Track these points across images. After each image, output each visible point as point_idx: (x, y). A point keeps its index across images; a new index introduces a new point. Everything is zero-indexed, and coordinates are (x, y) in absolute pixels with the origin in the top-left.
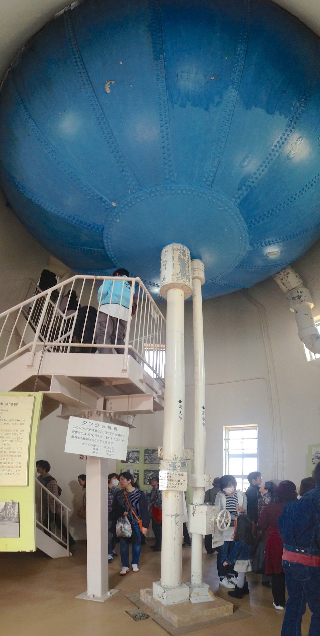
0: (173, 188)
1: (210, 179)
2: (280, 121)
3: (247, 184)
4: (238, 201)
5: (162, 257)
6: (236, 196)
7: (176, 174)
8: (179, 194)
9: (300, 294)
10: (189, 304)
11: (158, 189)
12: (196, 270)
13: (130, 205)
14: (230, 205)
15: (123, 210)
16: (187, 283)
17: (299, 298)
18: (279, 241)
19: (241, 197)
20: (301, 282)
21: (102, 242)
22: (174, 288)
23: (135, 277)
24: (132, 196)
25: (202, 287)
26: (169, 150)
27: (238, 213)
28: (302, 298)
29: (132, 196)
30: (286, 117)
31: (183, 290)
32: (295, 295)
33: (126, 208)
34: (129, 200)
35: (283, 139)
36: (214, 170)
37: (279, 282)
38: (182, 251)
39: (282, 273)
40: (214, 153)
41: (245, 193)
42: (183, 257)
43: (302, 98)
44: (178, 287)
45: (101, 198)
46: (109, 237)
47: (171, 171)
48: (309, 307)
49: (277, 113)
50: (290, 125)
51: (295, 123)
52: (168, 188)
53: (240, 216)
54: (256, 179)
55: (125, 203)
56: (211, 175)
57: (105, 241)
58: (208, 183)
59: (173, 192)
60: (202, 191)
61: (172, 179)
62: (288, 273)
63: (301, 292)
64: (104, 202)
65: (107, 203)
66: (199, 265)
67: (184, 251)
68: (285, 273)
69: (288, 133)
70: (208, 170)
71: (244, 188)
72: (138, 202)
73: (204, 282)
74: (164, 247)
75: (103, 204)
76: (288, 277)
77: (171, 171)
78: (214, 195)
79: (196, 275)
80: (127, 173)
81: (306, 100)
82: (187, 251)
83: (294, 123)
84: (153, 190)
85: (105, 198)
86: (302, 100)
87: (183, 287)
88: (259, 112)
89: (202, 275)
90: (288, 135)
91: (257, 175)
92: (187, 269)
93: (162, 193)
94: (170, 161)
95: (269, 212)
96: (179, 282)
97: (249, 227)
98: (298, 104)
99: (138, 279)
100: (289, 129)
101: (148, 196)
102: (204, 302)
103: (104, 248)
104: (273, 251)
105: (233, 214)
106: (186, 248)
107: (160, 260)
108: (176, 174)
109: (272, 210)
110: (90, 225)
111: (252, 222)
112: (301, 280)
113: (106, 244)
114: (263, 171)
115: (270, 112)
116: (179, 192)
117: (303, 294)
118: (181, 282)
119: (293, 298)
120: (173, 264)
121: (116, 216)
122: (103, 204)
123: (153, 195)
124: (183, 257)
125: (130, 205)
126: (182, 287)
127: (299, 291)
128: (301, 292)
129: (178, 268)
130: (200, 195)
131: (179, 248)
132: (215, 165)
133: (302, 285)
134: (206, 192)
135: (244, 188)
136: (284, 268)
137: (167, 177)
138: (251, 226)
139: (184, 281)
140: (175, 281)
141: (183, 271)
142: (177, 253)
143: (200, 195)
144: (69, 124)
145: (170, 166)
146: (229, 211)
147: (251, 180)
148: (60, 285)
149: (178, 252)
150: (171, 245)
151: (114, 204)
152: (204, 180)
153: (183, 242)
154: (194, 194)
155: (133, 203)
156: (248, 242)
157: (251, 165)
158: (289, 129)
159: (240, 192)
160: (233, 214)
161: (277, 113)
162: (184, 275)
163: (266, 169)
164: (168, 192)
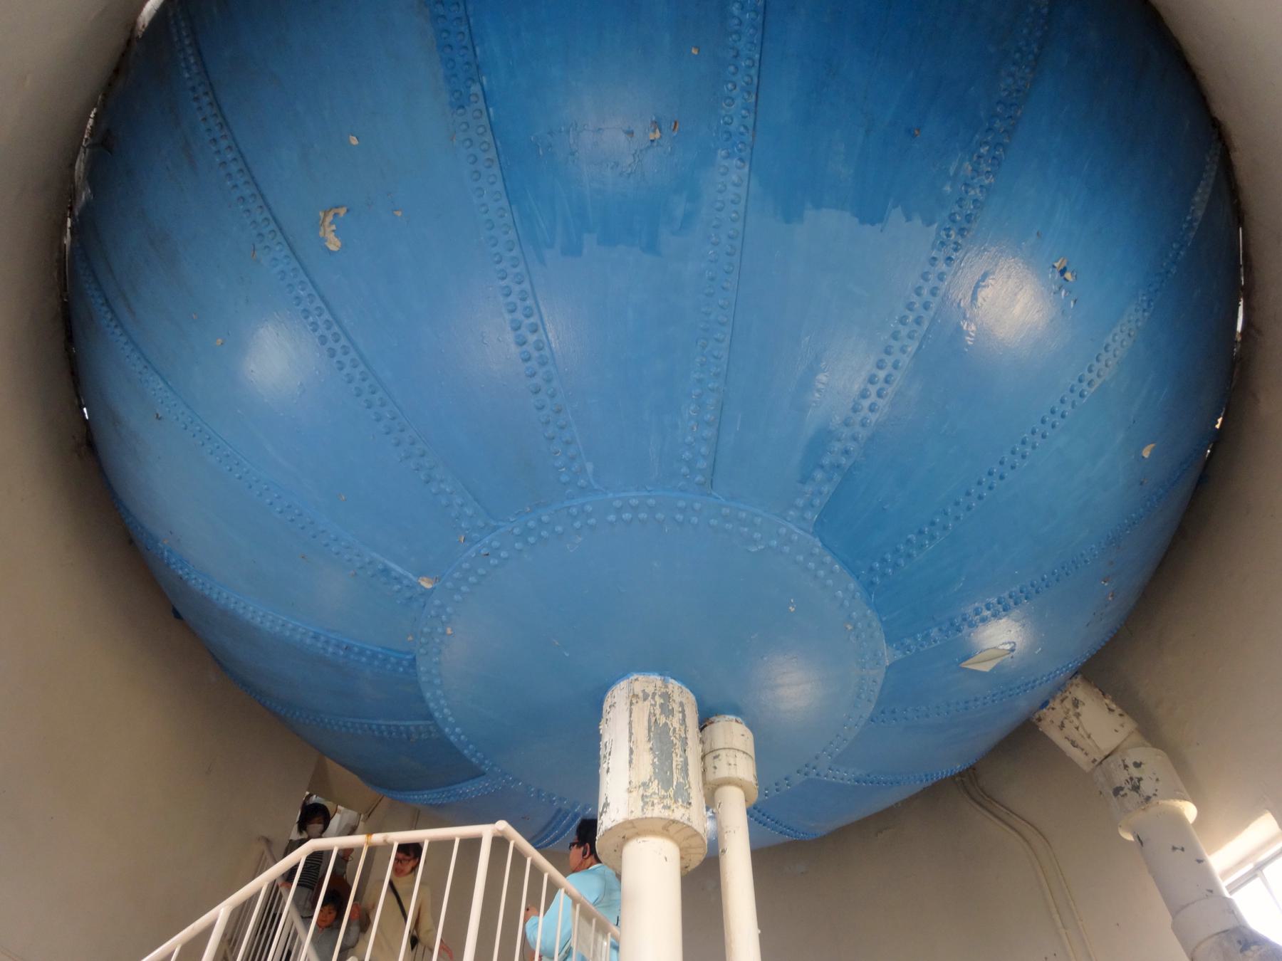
0: (589, 508)
1: (702, 464)
2: (908, 237)
3: (826, 461)
4: (812, 516)
5: (603, 727)
6: (800, 502)
7: (590, 467)
8: (611, 523)
9: (1135, 772)
10: (701, 883)
11: (545, 518)
12: (723, 753)
13: (472, 579)
14: (783, 531)
15: (457, 597)
16: (679, 813)
17: (1136, 788)
18: (987, 613)
19: (817, 502)
20: (1130, 725)
21: (422, 699)
22: (638, 834)
23: (492, 820)
24: (472, 553)
25: (750, 813)
26: (553, 396)
27: (817, 550)
28: (1146, 787)
29: (472, 553)
30: (930, 224)
31: (671, 838)
32: (1121, 778)
33: (464, 589)
34: (466, 566)
35: (925, 292)
36: (708, 433)
37: (1056, 736)
38: (659, 700)
39: (1056, 704)
40: (700, 381)
41: (826, 489)
42: (662, 720)
43: (981, 144)
44: (653, 833)
45: (386, 571)
46: (437, 681)
47: (573, 459)
48: (1179, 818)
49: (896, 215)
50: (943, 243)
51: (961, 231)
52: (574, 511)
53: (828, 559)
54: (855, 439)
55: (457, 575)
56: (703, 450)
57: (428, 695)
58: (699, 478)
59: (592, 521)
60: (681, 504)
61: (582, 482)
62: (1076, 703)
63: (1137, 765)
64: (398, 580)
65: (405, 582)
66: (733, 736)
67: (667, 697)
68: (1068, 704)
69: (942, 266)
70: (689, 439)
71: (819, 475)
72: (496, 566)
73: (755, 796)
74: (605, 692)
75: (397, 587)
76: (1078, 715)
77: (573, 459)
78: (725, 511)
79: (723, 771)
80: (442, 486)
81: (997, 145)
82: (682, 696)
83: (959, 230)
84: (531, 524)
85: (397, 569)
86: (983, 150)
87: (666, 828)
88: (832, 223)
89: (744, 769)
90: (941, 277)
91: (865, 412)
92: (677, 760)
93: (559, 529)
94: (562, 428)
95: (921, 532)
96: (650, 813)
97: (869, 586)
98: (968, 166)
99: (502, 825)
100: (941, 256)
101: (518, 545)
102: (761, 857)
103: (430, 716)
104: (1001, 637)
105: (801, 558)
106: (674, 686)
107: (599, 737)
108: (590, 467)
109: (933, 523)
110: (374, 655)
111: (872, 569)
112: (1127, 719)
113: (432, 705)
114: (872, 409)
115: (871, 214)
116: (612, 518)
117: (1145, 773)
118: (657, 812)
119: (1117, 791)
120: (631, 751)
121: (438, 616)
122: (397, 587)
123: (532, 540)
124: (662, 720)
125: (472, 579)
126: (665, 828)
127: (1129, 762)
128: (1137, 765)
129: (646, 762)
130: (679, 517)
131: (650, 690)
132: (708, 417)
133: (1136, 738)
134: (697, 506)
135: (819, 475)
136: (1061, 688)
137: (564, 478)
138: (872, 583)
139: (667, 807)
140: (638, 814)
141: (663, 772)
142: (642, 712)
143: (679, 517)
144: (275, 359)
145: (567, 443)
146: (787, 549)
147: (837, 446)
148: (333, 843)
149: (647, 703)
150: (623, 684)
151: (426, 584)
152: (684, 470)
153: (664, 669)
154: (660, 516)
155: (481, 571)
156: (879, 634)
157: (846, 379)
158: (941, 256)
159: (808, 488)
160: (801, 558)
161: (896, 215)
162: (666, 783)
163: (881, 402)
164: (577, 524)
